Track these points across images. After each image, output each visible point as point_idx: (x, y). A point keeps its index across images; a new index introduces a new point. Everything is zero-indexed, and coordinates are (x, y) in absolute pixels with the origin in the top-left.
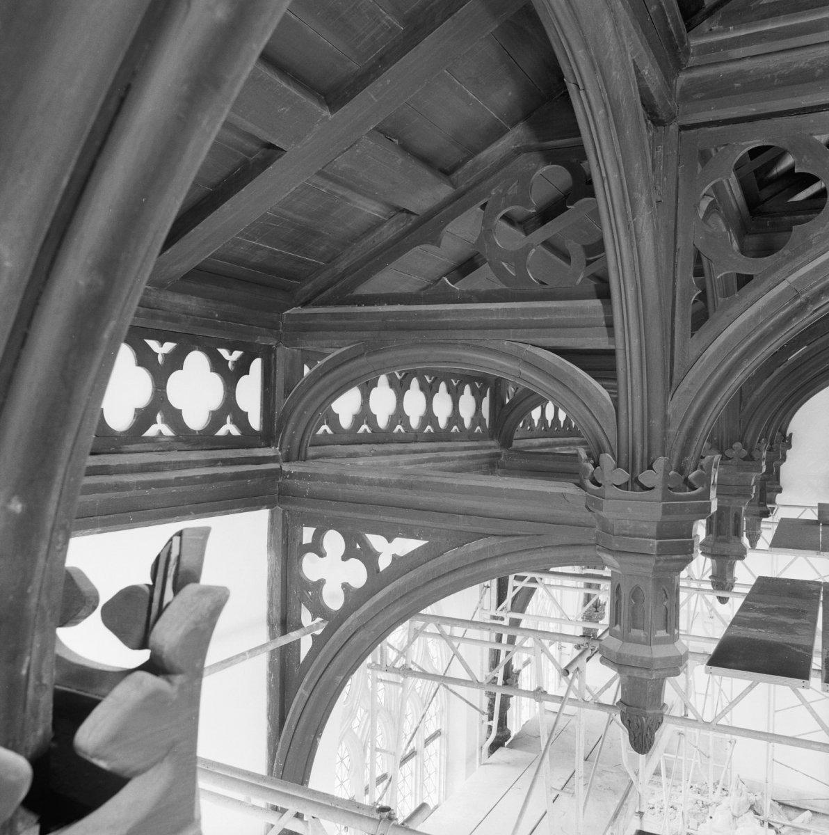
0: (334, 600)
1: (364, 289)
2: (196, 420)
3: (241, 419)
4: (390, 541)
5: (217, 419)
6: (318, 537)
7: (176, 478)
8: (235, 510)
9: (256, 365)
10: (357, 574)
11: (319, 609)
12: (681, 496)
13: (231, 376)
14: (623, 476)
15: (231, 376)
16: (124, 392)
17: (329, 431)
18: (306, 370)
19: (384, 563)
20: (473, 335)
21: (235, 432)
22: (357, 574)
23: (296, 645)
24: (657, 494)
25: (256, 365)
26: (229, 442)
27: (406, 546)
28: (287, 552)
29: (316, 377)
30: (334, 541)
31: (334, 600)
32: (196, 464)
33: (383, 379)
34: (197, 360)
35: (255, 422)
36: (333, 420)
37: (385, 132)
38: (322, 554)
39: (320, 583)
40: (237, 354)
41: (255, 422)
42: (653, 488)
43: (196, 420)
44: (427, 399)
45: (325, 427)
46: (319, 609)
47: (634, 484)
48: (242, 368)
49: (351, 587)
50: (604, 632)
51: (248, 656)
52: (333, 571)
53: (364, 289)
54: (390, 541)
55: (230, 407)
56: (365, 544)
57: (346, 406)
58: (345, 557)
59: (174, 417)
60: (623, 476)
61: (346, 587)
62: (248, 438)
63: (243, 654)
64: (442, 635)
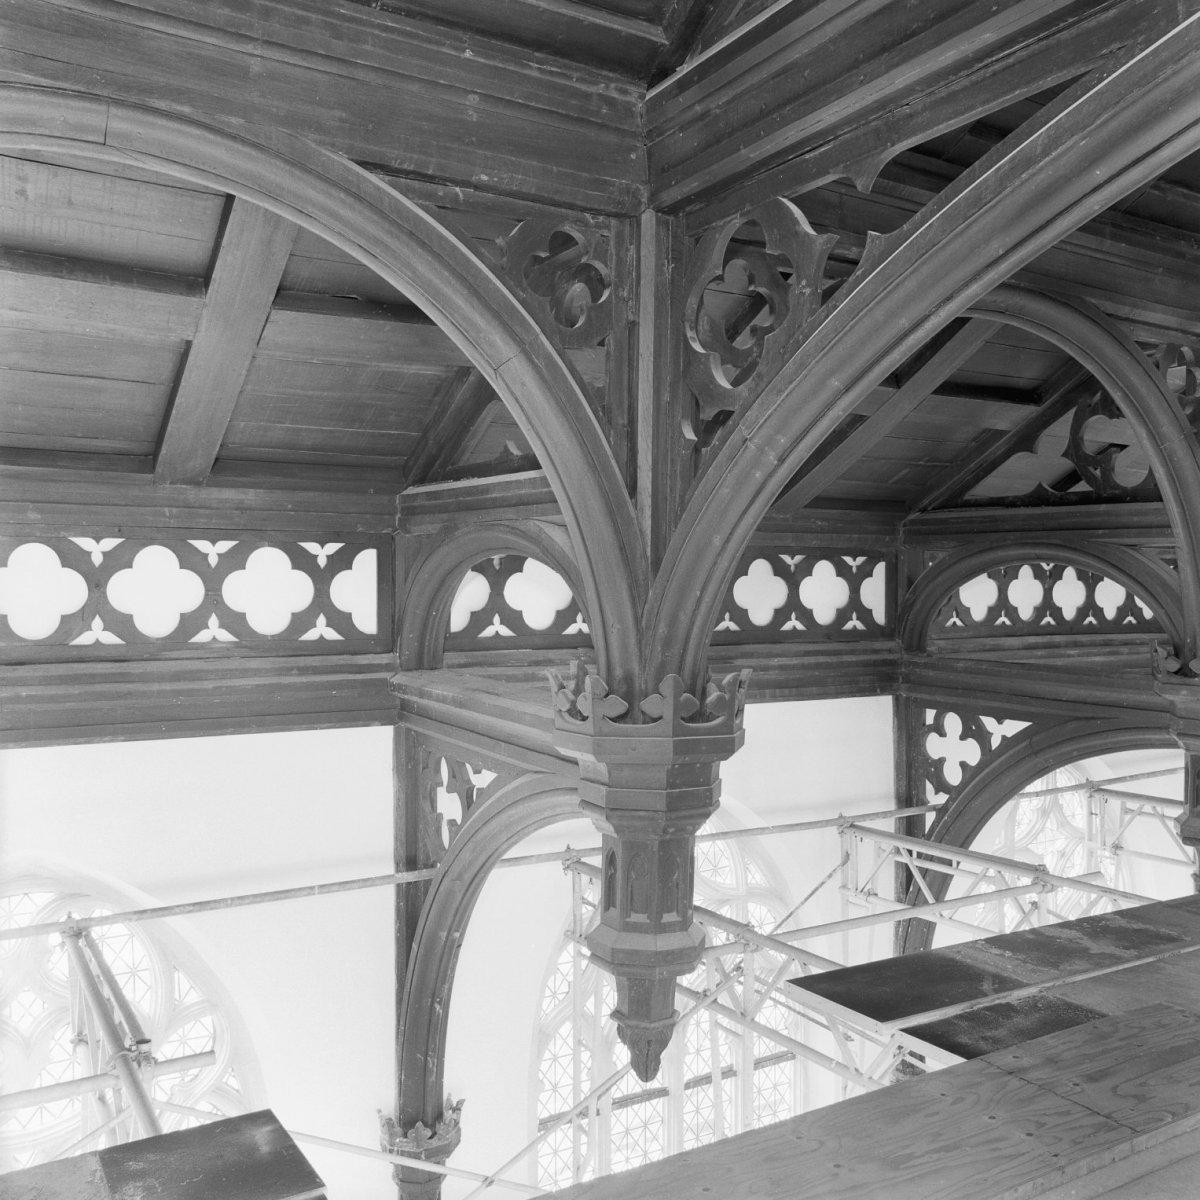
0: (953, 776)
1: (970, 495)
2: (824, 616)
3: (865, 615)
5: (842, 615)
6: (939, 719)
7: (215, 688)
8: (325, 725)
9: (880, 569)
10: (972, 753)
12: (698, 729)
13: (855, 580)
15: (855, 580)
21: (860, 626)
22: (972, 753)
23: (921, 818)
24: (667, 725)
25: (880, 569)
27: (1013, 727)
30: (953, 722)
31: (953, 776)
32: (257, 672)
34: (824, 569)
35: (880, 617)
36: (963, 613)
37: (286, 296)
38: (942, 734)
39: (942, 761)
40: (860, 560)
41: (880, 617)
42: (660, 718)
43: (824, 616)
44: (1087, 591)
46: (941, 786)
48: (866, 572)
49: (968, 765)
51: (317, 891)
52: (953, 749)
55: (855, 605)
56: (981, 727)
57: (977, 595)
58: (963, 737)
59: (806, 615)
61: (963, 765)
62: (873, 631)
63: (312, 888)
64: (1155, 815)
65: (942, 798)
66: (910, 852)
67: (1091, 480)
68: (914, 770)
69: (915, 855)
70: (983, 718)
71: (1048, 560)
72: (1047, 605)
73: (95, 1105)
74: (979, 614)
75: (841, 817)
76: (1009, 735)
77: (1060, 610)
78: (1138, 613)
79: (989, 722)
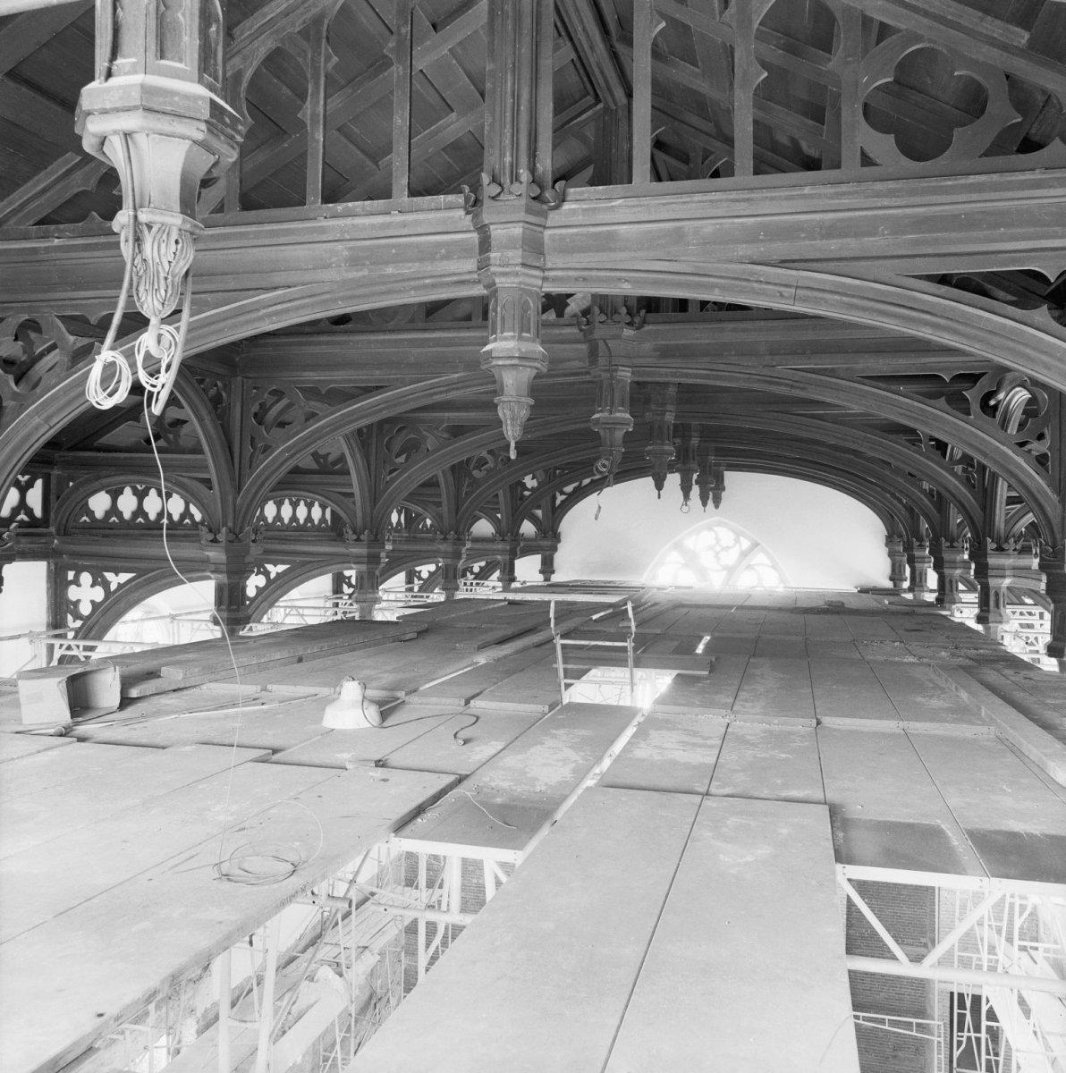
0: (85, 609)
1: (107, 439)
3: (30, 512)
4: (117, 575)
9: (39, 483)
10: (98, 594)
11: (420, 578)
14: (355, 537)
16: (270, 510)
17: (88, 520)
18: (71, 484)
19: (113, 587)
20: (309, 486)
21: (26, 518)
22: (98, 594)
25: (39, 483)
26: (140, 526)
27: (281, 568)
28: (58, 585)
29: (76, 488)
30: (86, 578)
31: (85, 609)
33: (287, 501)
35: (38, 513)
36: (91, 513)
38: (79, 585)
40: (27, 477)
41: (38, 513)
45: (85, 518)
46: (77, 616)
47: (358, 540)
48: (30, 484)
50: (205, 611)
52: (85, 593)
53: (107, 439)
54: (117, 575)
57: (99, 503)
60: (355, 537)
65: (79, 623)
66: (78, 647)
67: (167, 440)
68: (60, 608)
69: (81, 648)
70: (106, 574)
71: (140, 483)
72: (140, 511)
73: (44, 651)
74: (99, 514)
75: (31, 632)
76: (122, 582)
77: (147, 514)
78: (192, 517)
79: (269, 567)
